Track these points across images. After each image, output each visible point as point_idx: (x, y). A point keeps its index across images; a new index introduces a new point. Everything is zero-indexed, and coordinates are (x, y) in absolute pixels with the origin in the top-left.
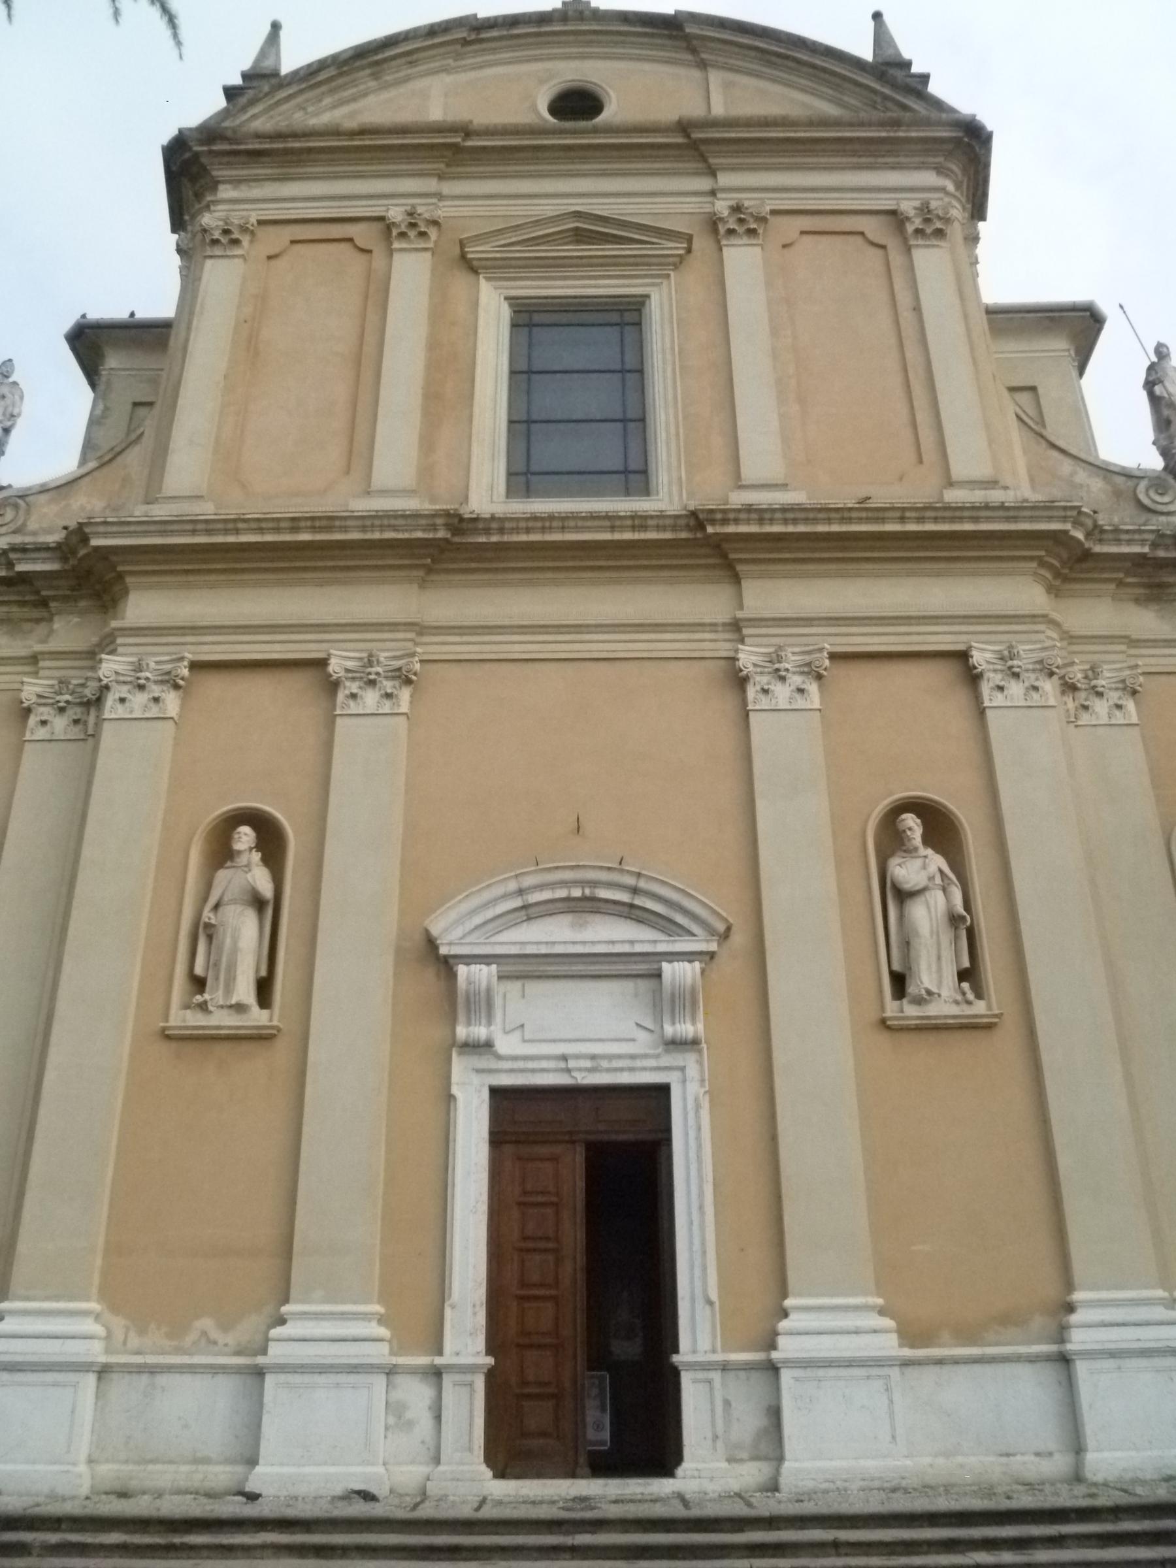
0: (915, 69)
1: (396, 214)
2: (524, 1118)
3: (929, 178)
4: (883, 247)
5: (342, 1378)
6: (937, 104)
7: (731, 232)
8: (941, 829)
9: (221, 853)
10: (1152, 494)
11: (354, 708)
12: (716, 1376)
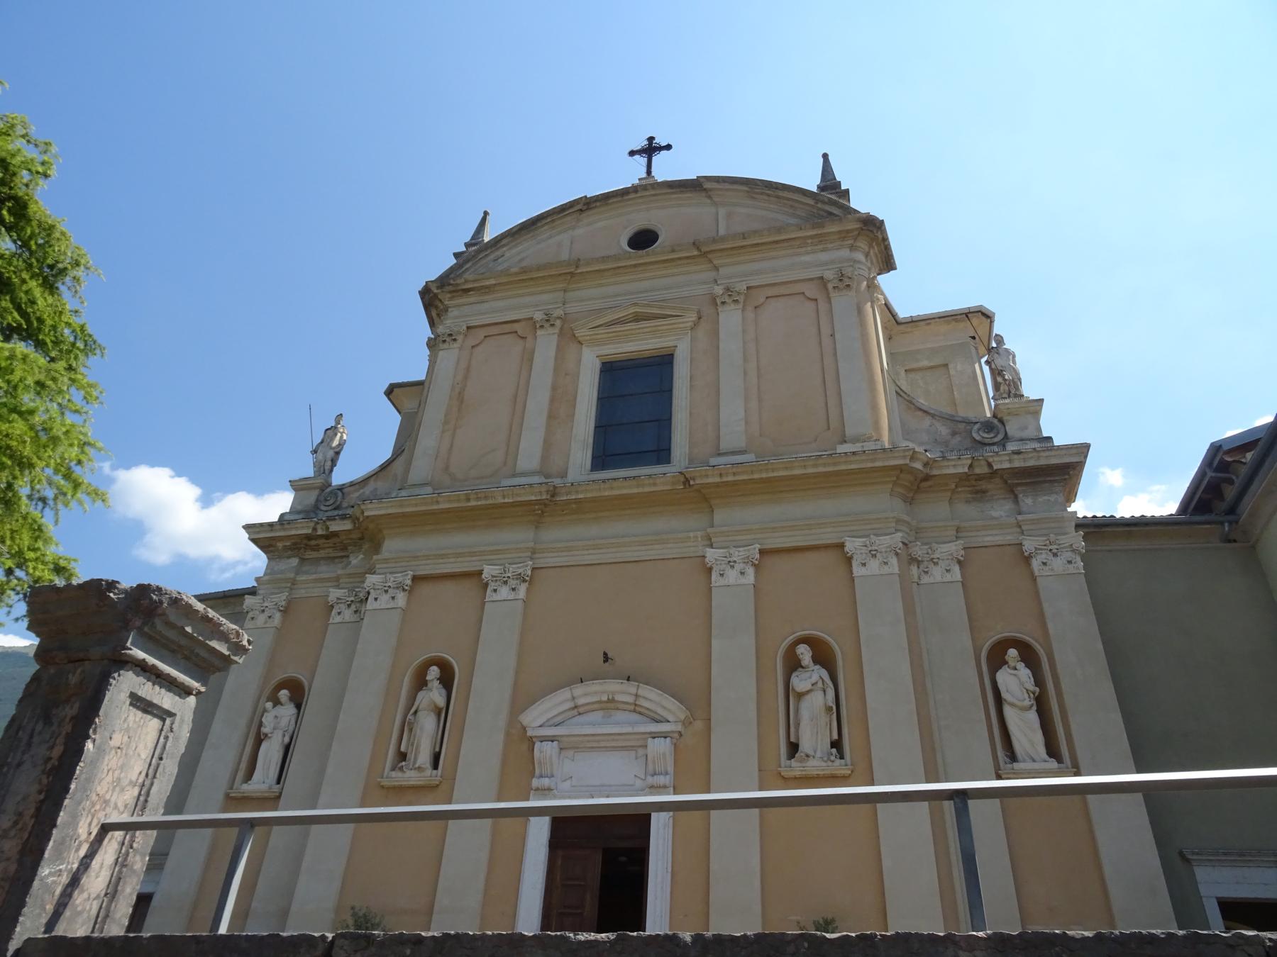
1: (538, 316)
2: (570, 830)
3: (845, 253)
7: (723, 303)
8: (824, 657)
9: (420, 683)
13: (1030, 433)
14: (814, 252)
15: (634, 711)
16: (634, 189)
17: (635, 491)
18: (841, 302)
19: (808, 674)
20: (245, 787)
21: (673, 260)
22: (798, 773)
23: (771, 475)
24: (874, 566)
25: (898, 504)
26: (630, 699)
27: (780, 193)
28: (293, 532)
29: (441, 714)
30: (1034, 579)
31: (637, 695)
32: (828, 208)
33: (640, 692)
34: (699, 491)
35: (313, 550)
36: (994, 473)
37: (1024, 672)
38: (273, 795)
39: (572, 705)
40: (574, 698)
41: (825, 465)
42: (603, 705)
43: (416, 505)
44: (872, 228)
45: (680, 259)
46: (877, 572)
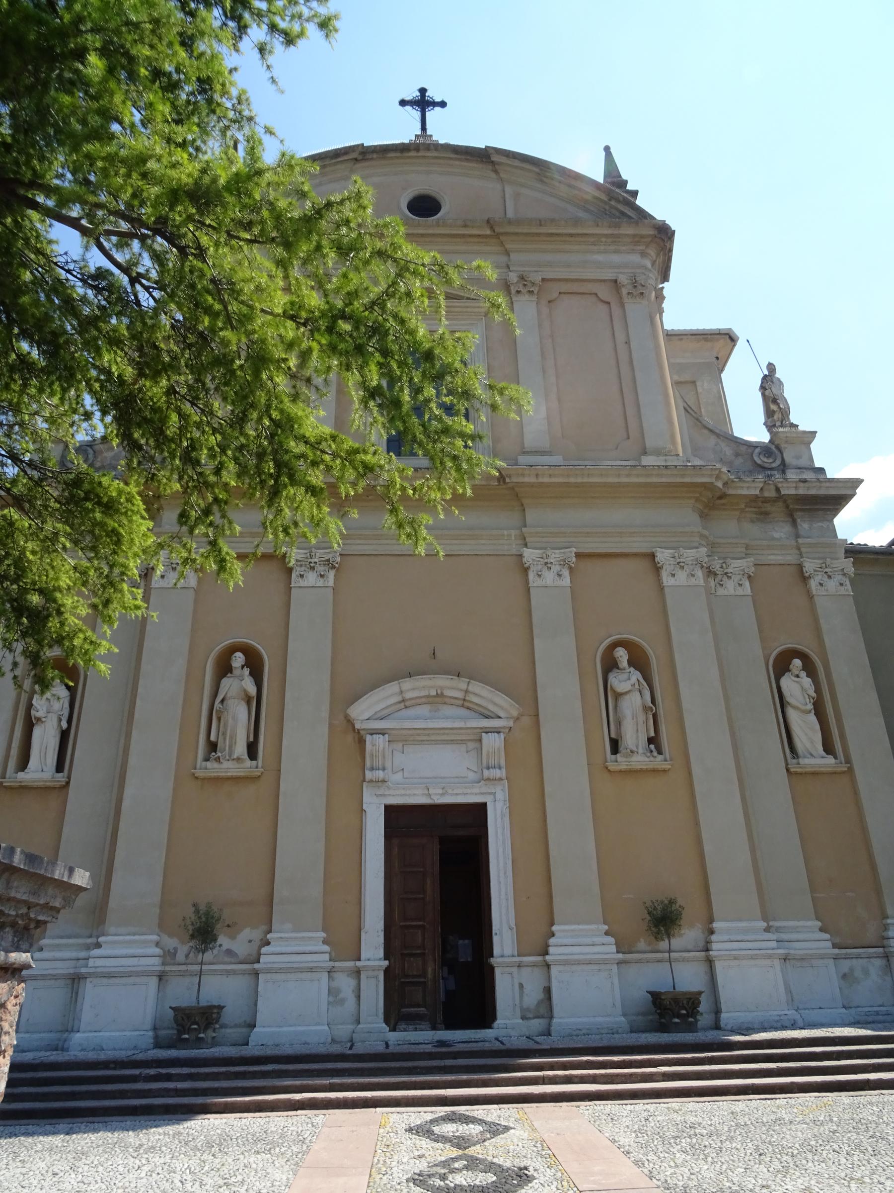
0: (629, 187)
3: (635, 258)
4: (609, 303)
5: (304, 976)
6: (643, 215)
7: (518, 292)
9: (224, 669)
10: (761, 457)
11: (302, 583)
12: (515, 970)
13: (803, 462)
14: (605, 252)
15: (463, 706)
16: (402, 149)
18: (633, 308)
19: (625, 676)
20: (21, 775)
21: (463, 236)
22: (623, 767)
23: (585, 480)
24: (682, 577)
25: (695, 518)
26: (460, 695)
29: (255, 703)
30: (811, 597)
31: (466, 691)
32: (621, 207)
33: (470, 688)
34: (513, 489)
36: (780, 497)
37: (807, 681)
38: (58, 784)
39: (400, 698)
40: (401, 692)
41: (638, 476)
42: (431, 700)
44: (663, 235)
45: (470, 236)
46: (685, 583)
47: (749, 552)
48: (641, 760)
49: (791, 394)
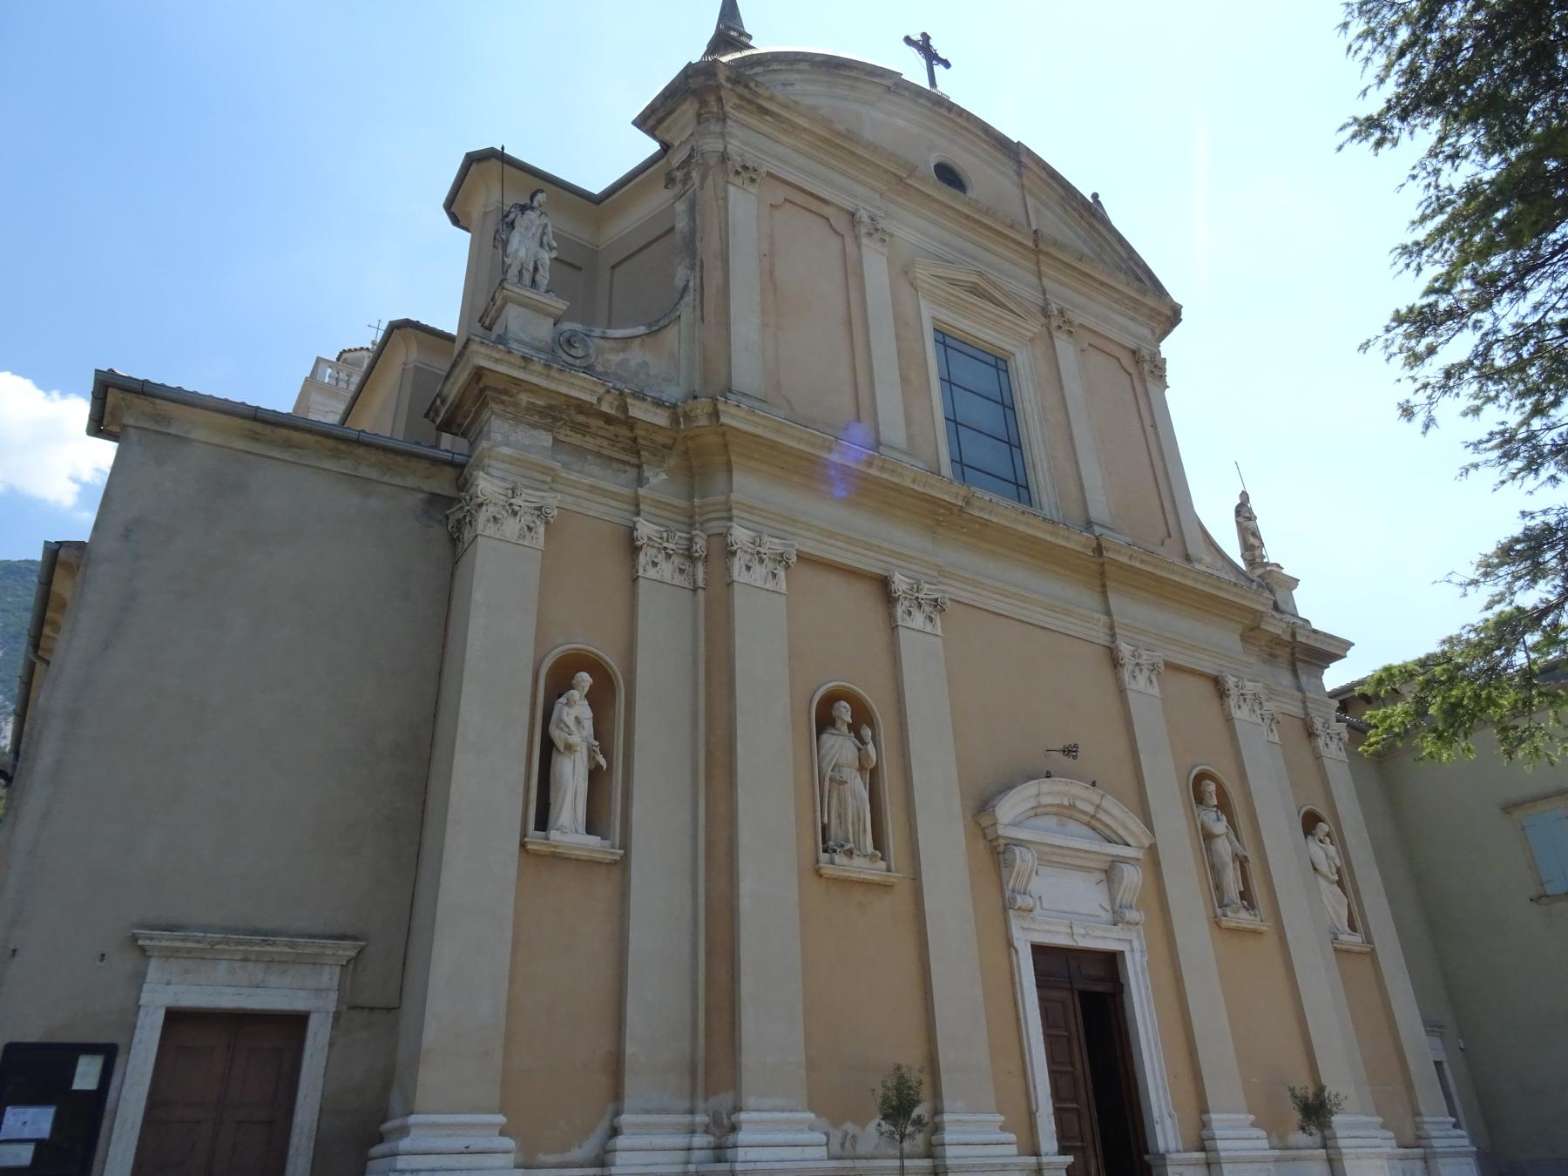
15: (1088, 824)
17: (1048, 538)
21: (1007, 237)
27: (1095, 223)
28: (564, 390)
33: (1104, 803)
35: (573, 429)
43: (800, 440)
45: (1014, 241)
47: (555, 486)
48: (862, 867)
49: (1264, 525)
